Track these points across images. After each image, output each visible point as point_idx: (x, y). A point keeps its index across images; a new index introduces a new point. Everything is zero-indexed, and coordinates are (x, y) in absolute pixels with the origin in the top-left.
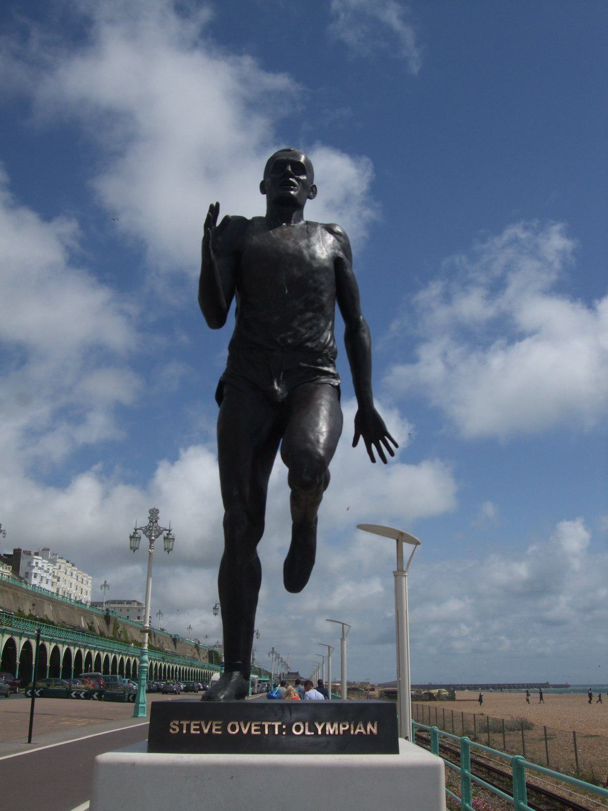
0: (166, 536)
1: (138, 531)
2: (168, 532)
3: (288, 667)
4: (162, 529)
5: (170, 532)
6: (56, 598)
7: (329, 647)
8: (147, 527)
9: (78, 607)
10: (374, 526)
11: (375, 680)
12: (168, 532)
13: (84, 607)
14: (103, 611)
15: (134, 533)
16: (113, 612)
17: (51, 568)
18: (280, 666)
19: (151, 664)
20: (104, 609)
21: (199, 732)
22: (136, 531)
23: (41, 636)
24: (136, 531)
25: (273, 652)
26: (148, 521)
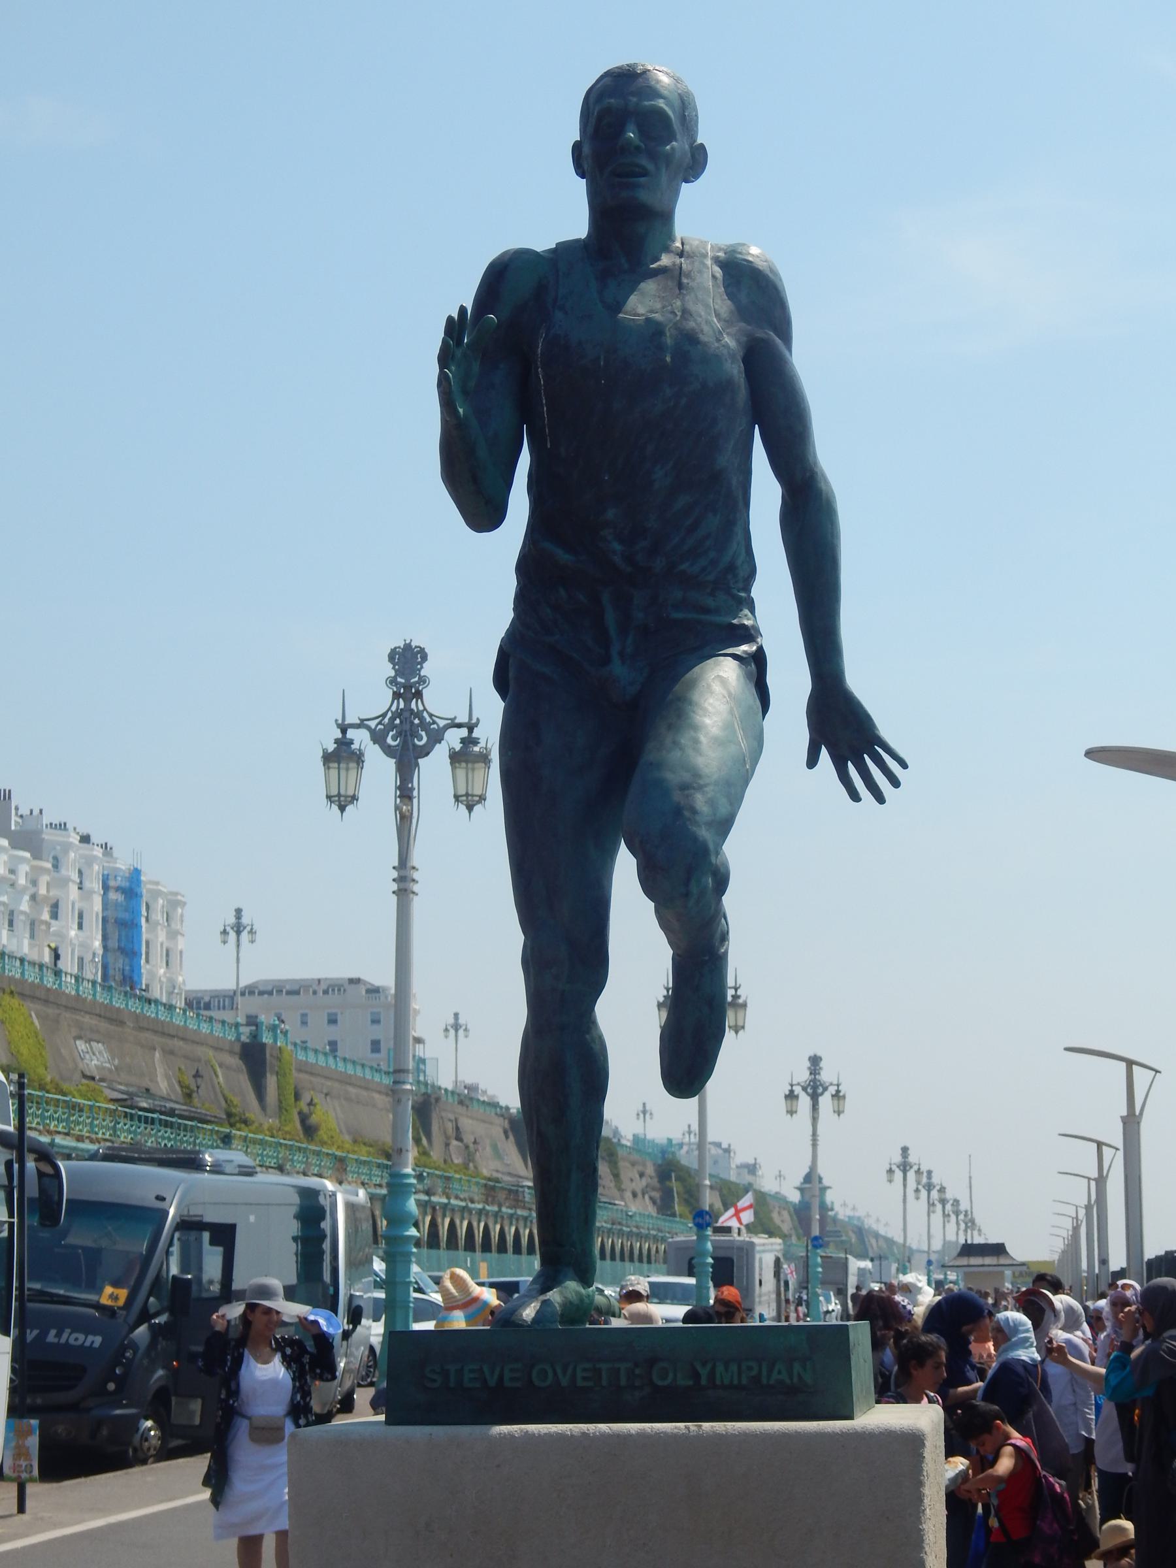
0: (458, 747)
1: (351, 734)
2: (464, 732)
3: (971, 1224)
4: (442, 723)
5: (471, 730)
6: (49, 981)
7: (1100, 1145)
8: (384, 715)
9: (137, 1017)
10: (895, 776)
11: (1020, 1251)
12: (464, 732)
13: (163, 1016)
14: (237, 1025)
15: (337, 741)
16: (273, 1029)
17: (24, 869)
18: (937, 1217)
19: (433, 1224)
20: (241, 1019)
21: (98, 1340)
22: (344, 731)
23: (29, 1133)
24: (344, 731)
25: (905, 1167)
26: (389, 694)
